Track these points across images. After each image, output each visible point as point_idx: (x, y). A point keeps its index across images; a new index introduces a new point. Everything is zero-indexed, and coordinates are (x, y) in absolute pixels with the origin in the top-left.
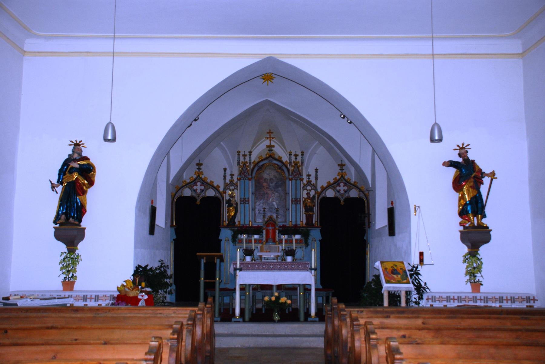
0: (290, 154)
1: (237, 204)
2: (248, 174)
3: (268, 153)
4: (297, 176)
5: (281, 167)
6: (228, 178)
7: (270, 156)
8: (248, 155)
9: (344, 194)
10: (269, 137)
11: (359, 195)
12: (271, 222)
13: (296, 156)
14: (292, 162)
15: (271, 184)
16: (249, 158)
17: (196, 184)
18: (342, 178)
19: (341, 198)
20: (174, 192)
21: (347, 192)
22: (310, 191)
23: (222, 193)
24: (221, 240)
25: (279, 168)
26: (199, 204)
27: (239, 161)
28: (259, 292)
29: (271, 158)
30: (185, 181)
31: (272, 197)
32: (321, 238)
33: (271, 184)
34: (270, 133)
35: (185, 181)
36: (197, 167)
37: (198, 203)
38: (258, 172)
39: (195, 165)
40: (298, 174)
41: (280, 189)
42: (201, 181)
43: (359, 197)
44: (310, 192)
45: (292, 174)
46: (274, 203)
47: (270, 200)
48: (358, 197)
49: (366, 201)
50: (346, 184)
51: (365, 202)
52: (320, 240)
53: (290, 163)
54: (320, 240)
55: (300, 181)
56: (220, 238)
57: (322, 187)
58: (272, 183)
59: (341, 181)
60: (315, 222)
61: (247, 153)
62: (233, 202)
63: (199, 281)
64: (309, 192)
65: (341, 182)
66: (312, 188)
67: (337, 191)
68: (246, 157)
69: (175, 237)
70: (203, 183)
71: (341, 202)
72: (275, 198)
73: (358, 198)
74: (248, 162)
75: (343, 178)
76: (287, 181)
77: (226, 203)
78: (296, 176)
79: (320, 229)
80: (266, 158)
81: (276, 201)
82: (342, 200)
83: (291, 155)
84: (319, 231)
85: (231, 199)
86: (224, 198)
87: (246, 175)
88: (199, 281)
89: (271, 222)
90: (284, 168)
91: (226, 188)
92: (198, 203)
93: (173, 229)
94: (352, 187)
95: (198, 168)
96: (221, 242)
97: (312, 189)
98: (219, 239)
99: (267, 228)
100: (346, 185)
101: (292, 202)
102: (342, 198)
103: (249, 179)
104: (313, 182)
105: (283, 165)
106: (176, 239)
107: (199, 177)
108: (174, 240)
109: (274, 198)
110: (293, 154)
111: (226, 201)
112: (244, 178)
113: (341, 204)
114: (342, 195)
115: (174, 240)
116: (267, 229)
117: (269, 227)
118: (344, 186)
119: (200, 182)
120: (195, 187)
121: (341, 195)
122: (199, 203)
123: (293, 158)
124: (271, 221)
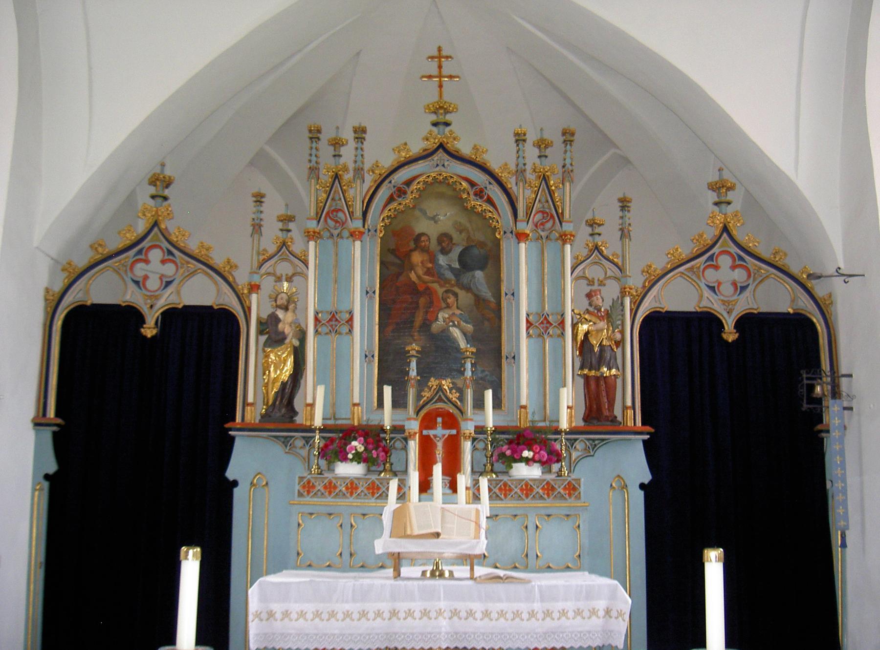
0: (520, 139)
1: (302, 336)
2: (351, 214)
3: (430, 133)
4: (549, 225)
5: (481, 191)
6: (272, 232)
7: (441, 146)
8: (352, 144)
9: (735, 297)
10: (435, 72)
11: (793, 301)
12: (440, 405)
13: (542, 145)
14: (529, 168)
15: (442, 260)
16: (353, 152)
17: (143, 257)
18: (725, 235)
19: (725, 314)
20: (58, 287)
21: (747, 293)
22: (602, 283)
23: (246, 291)
24: (235, 483)
25: (476, 194)
26: (153, 337)
27: (313, 163)
28: (714, 282)
29: (441, 153)
30: (100, 245)
31: (448, 306)
32: (647, 477)
33: (442, 260)
34: (440, 57)
35: (100, 245)
36: (280, 225)
37: (149, 330)
38: (391, 206)
39: (276, 219)
40: (552, 216)
41: (479, 274)
42: (165, 245)
43: (794, 310)
44: (356, 146)
45: (528, 215)
46: (456, 333)
47: (440, 322)
48: (791, 311)
49: (820, 327)
50: (741, 258)
51: (819, 328)
52: (642, 486)
53: (520, 173)
54: (642, 486)
55: (560, 242)
56: (231, 473)
57: (647, 270)
58: (445, 252)
59: (722, 246)
60: (625, 408)
61: (348, 135)
62: (286, 327)
63: (429, 479)
64: (596, 287)
65: (722, 253)
66: (609, 273)
67: (708, 286)
68: (343, 151)
69: (52, 467)
70: (170, 253)
71: (724, 328)
72: (458, 312)
73: (789, 313)
74: (351, 166)
75: (730, 236)
76: (507, 245)
77: (260, 332)
78: (542, 224)
79: (647, 437)
80: (426, 155)
81: (463, 324)
82: (729, 323)
83: (524, 141)
84: (641, 446)
85: (280, 314)
86: (250, 309)
87: (344, 219)
88: (429, 479)
89: (440, 405)
90: (495, 192)
91: (263, 270)
92: (149, 330)
93: (47, 434)
94: (767, 271)
95: (281, 227)
96: (236, 491)
97: (607, 278)
98: (226, 479)
99: (425, 432)
100: (171, 257)
101: (316, 326)
102: (440, 396)
103: (355, 235)
104: (611, 244)
105: (490, 183)
106: (56, 474)
107: (156, 229)
108: (47, 477)
109: (454, 314)
110: (532, 137)
111: (260, 322)
112: (336, 232)
113: (725, 336)
114: (729, 302)
115: (47, 477)
116: (428, 437)
117: (433, 427)
118: (163, 262)
119: (161, 248)
120: (140, 269)
121: (724, 302)
122: (155, 332)
123: (531, 153)
124: (440, 400)
